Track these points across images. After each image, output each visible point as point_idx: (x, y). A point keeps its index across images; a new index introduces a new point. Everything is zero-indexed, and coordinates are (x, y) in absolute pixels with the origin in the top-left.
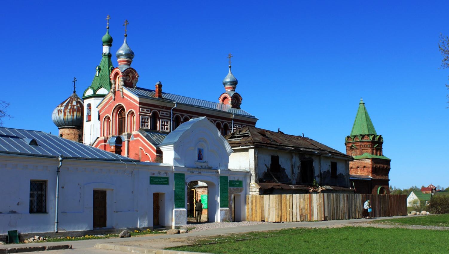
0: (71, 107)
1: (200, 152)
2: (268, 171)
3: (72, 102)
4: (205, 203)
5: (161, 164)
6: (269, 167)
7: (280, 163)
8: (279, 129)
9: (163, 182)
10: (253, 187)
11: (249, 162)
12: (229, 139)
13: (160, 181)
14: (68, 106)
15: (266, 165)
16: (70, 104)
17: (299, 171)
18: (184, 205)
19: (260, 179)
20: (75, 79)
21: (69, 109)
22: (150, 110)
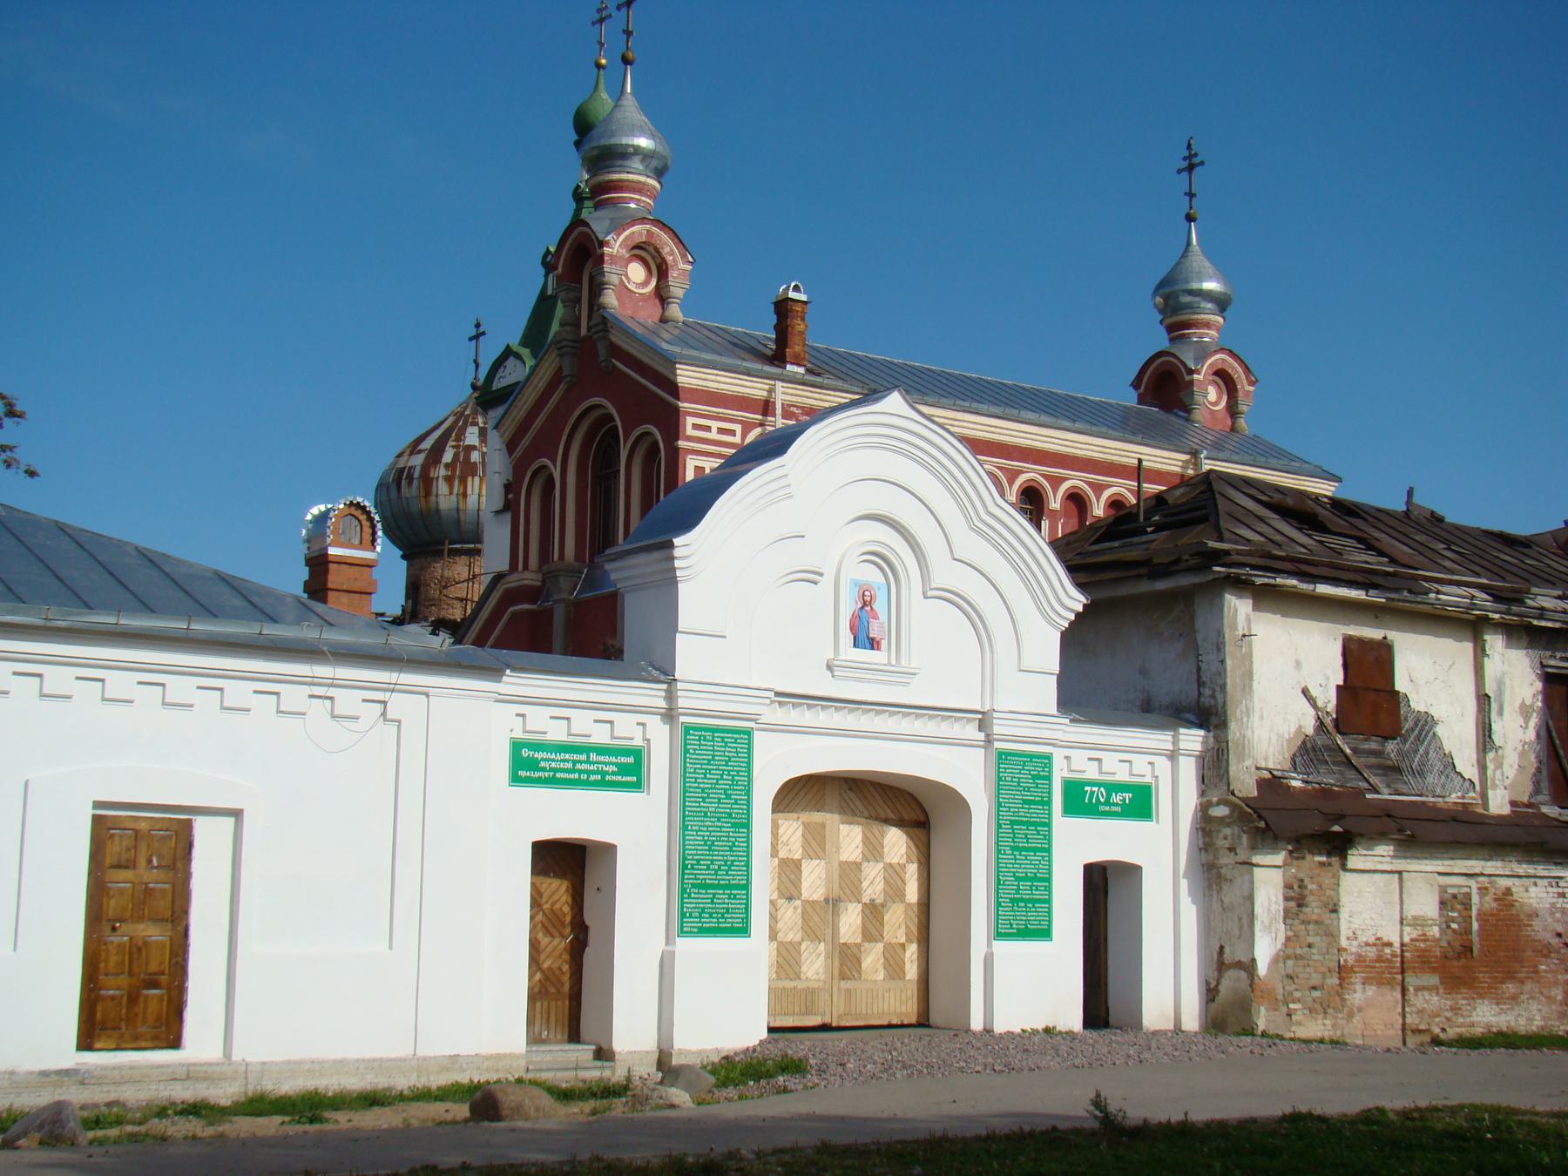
0: (456, 456)
1: (865, 604)
2: (1320, 725)
3: (461, 435)
6: (1331, 706)
7: (1401, 684)
8: (1410, 493)
11: (1199, 669)
12: (1094, 543)
13: (580, 772)
14: (443, 451)
15: (1305, 692)
16: (451, 443)
17: (1531, 735)
18: (747, 920)
19: (1266, 775)
20: (478, 326)
21: (447, 466)
22: (738, 428)
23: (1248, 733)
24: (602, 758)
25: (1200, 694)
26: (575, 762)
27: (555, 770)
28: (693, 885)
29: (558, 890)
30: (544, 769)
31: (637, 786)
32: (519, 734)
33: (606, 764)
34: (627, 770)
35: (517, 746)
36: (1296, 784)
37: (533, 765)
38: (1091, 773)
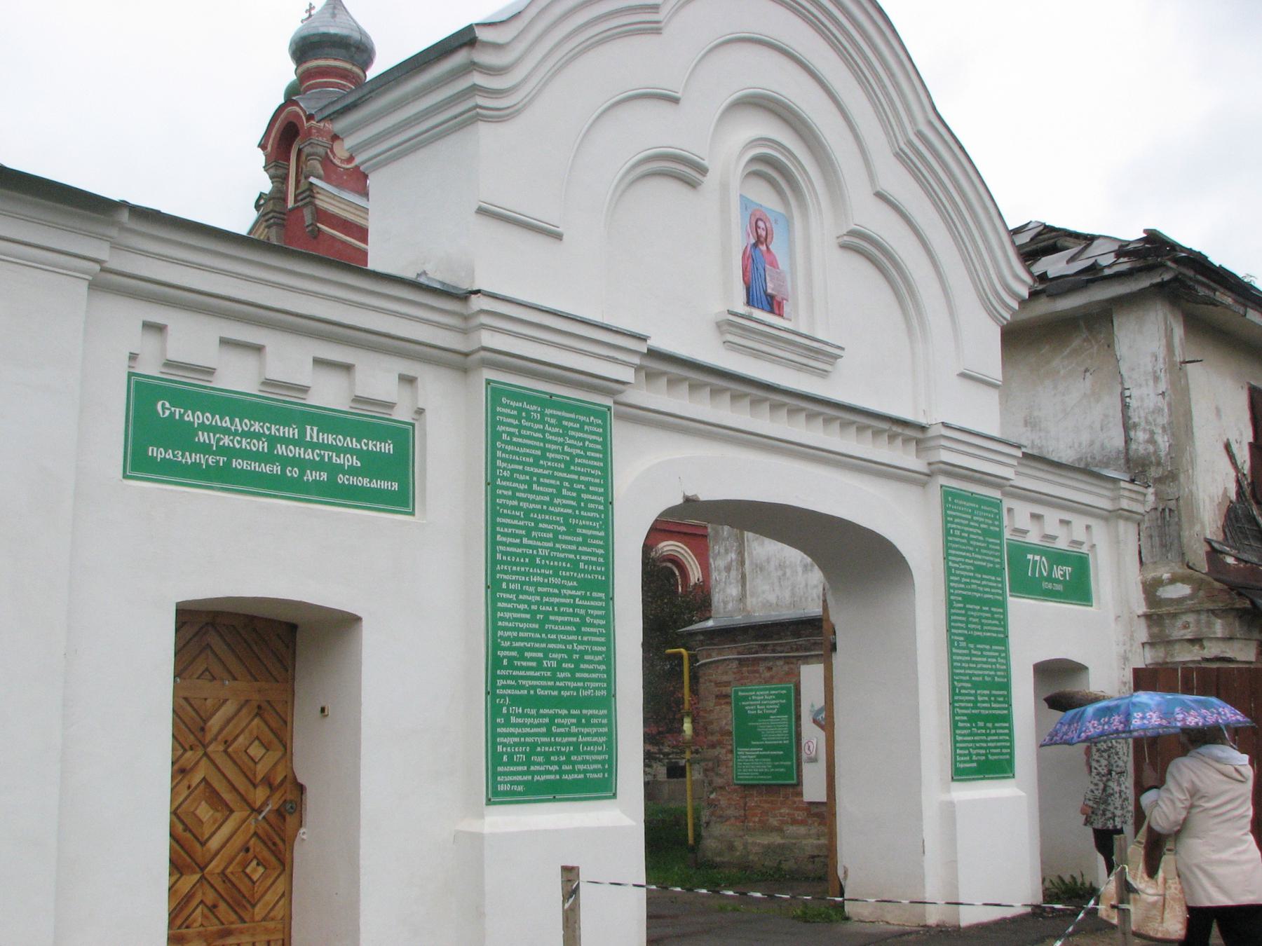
4: (766, 747)
5: (850, 927)
9: (335, 470)
10: (1171, 601)
11: (1125, 407)
13: (286, 462)
15: (1227, 447)
23: (1194, 488)
24: (329, 439)
25: (1128, 440)
26: (273, 441)
27: (230, 453)
28: (515, 700)
29: (227, 703)
30: (205, 449)
31: (402, 500)
32: (150, 367)
33: (339, 451)
34: (379, 469)
35: (143, 393)
36: (1230, 560)
37: (181, 436)
38: (1033, 538)
